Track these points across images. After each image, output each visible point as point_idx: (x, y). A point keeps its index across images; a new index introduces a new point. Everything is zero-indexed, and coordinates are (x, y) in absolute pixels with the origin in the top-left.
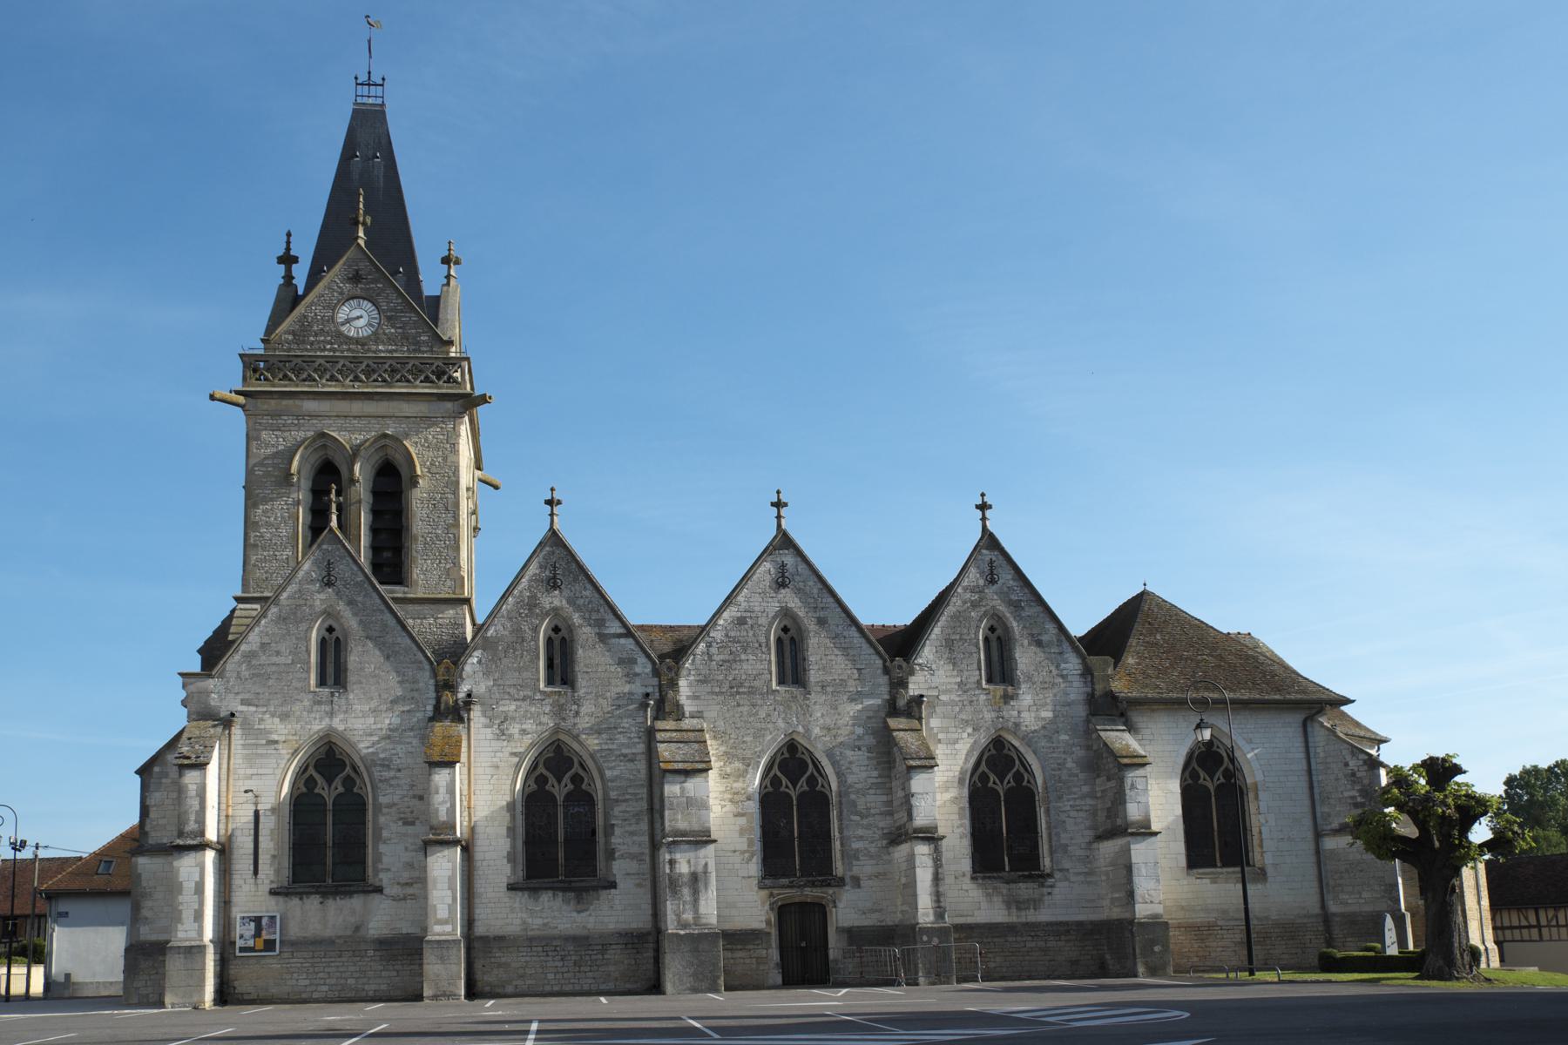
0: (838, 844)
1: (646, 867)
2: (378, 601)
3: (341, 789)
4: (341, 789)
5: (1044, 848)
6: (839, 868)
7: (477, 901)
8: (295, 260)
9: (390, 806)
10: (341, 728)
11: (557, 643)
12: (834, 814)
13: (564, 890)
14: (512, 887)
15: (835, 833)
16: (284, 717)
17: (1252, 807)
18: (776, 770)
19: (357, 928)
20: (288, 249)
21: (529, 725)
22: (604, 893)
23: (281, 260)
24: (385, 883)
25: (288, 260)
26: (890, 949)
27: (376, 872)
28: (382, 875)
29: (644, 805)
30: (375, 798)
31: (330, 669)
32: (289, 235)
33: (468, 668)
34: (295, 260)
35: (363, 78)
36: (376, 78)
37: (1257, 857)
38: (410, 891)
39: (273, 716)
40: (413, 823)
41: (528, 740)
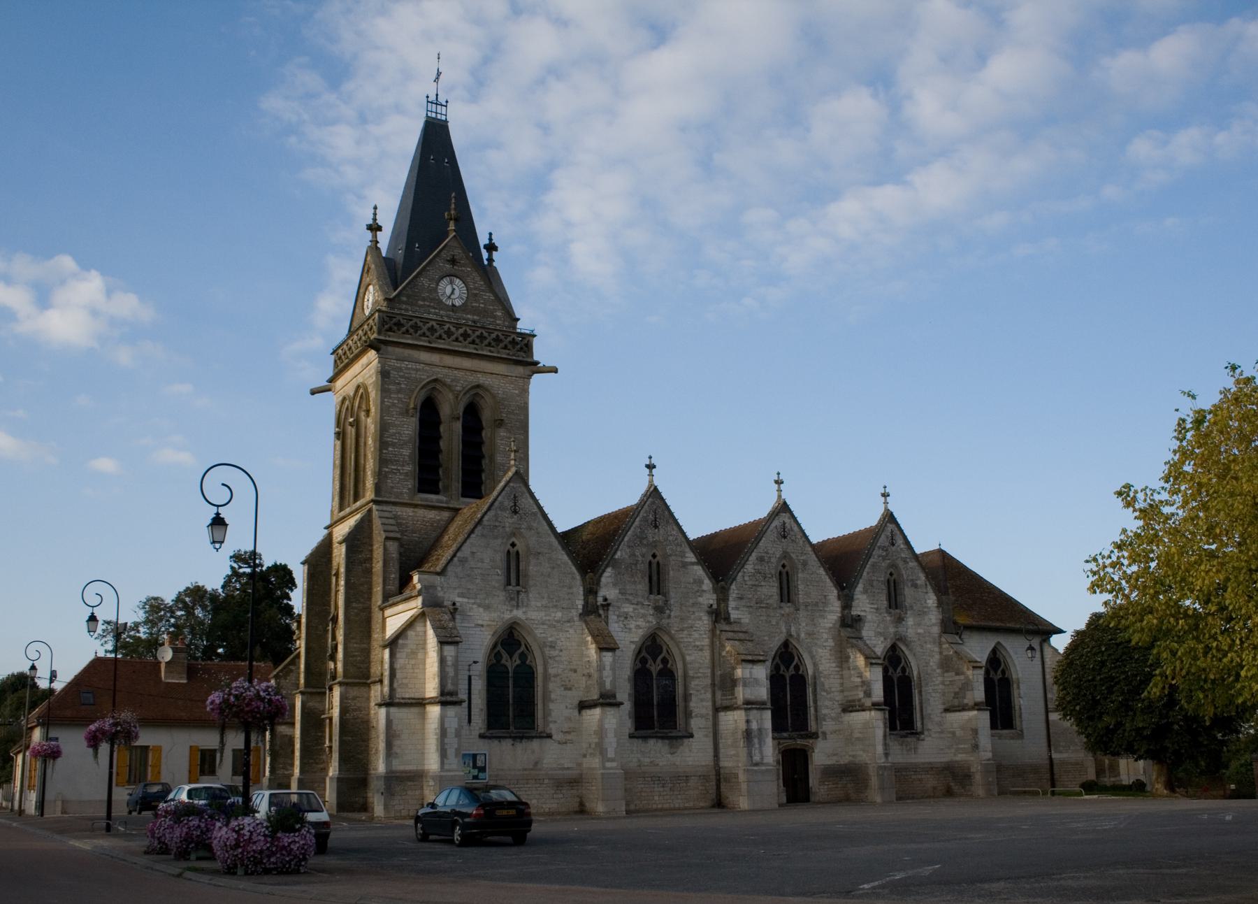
0: (812, 709)
1: (710, 723)
2: (547, 528)
3: (518, 662)
4: (518, 662)
5: (917, 716)
6: (812, 726)
7: (496, 742)
8: (379, 228)
9: (556, 676)
10: (523, 617)
11: (654, 566)
12: (810, 690)
13: (662, 738)
14: (631, 736)
15: (810, 702)
16: (487, 608)
17: (1015, 692)
18: (777, 659)
19: (536, 763)
20: (375, 219)
21: (641, 622)
22: (686, 741)
23: (370, 228)
24: (553, 732)
25: (375, 228)
26: (850, 778)
27: (546, 723)
28: (551, 725)
29: (709, 681)
30: (545, 669)
31: (513, 575)
32: (375, 208)
33: (603, 580)
34: (379, 228)
35: (433, 98)
36: (442, 100)
37: (1018, 723)
38: (569, 737)
39: (479, 606)
40: (570, 689)
41: (641, 632)
